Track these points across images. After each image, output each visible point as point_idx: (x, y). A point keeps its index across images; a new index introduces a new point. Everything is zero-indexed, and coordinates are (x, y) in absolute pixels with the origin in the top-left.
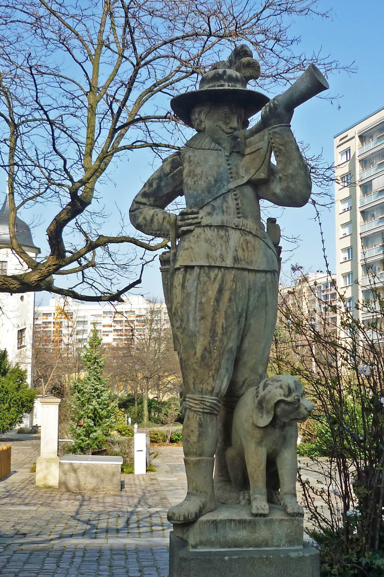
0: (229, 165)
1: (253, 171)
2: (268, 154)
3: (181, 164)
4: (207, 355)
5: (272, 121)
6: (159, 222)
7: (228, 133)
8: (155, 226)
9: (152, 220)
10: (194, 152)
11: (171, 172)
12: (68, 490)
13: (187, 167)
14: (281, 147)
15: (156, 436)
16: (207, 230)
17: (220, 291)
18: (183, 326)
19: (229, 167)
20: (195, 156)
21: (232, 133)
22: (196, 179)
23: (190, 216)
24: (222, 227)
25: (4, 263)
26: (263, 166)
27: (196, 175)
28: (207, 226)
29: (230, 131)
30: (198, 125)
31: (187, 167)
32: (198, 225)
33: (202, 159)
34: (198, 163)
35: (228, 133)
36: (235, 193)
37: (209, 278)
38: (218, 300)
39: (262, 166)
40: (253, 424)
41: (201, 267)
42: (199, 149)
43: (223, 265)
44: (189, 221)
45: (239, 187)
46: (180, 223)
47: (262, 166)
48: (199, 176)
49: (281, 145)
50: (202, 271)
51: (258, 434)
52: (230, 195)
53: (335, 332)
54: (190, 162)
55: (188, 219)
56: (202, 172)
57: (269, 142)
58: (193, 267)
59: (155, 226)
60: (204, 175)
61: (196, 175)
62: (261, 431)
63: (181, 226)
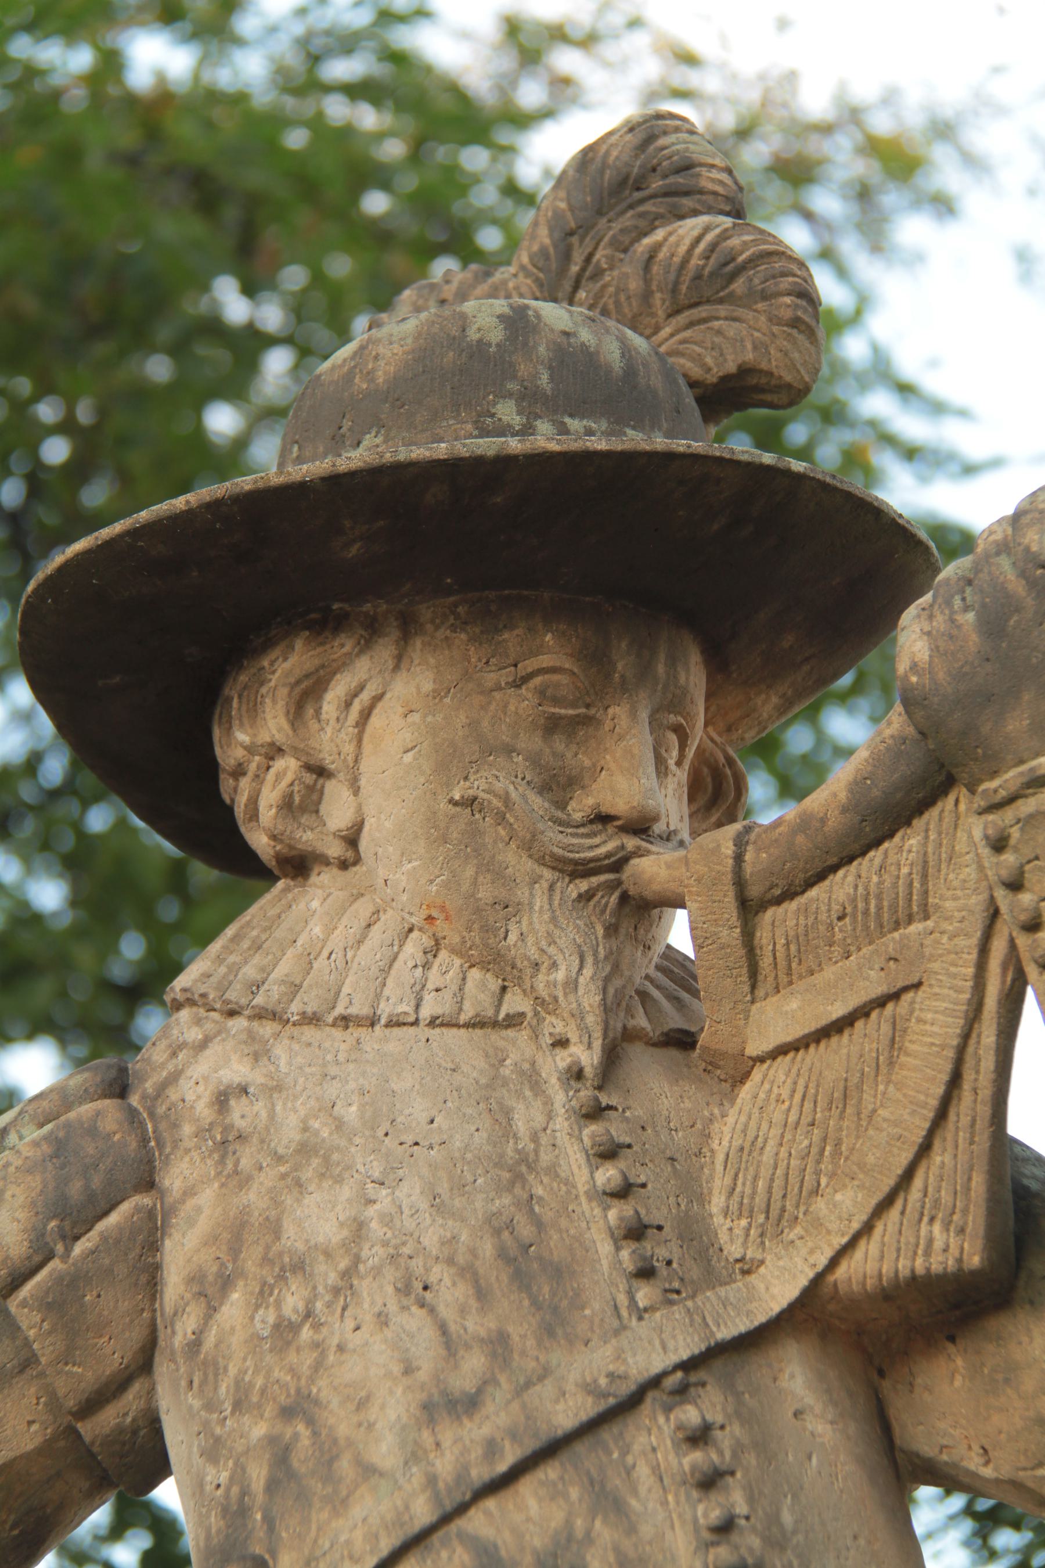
0: (609, 1153)
2: (988, 1035)
4: (438, 1022)
7: (580, 870)
10: (259, 1054)
13: (207, 1197)
15: (561, 829)
19: (608, 1175)
20: (275, 1088)
21: (618, 864)
26: (939, 1157)
27: (299, 1266)
29: (606, 845)
30: (287, 806)
31: (207, 1197)
33: (351, 1113)
34: (305, 1149)
35: (580, 870)
36: (690, 1415)
39: (925, 1149)
42: (312, 1020)
45: (718, 1364)
47: (925, 1149)
48: (328, 1274)
52: (640, 1441)
53: (218, 1248)
56: (359, 1229)
57: (995, 914)
60: (373, 1254)
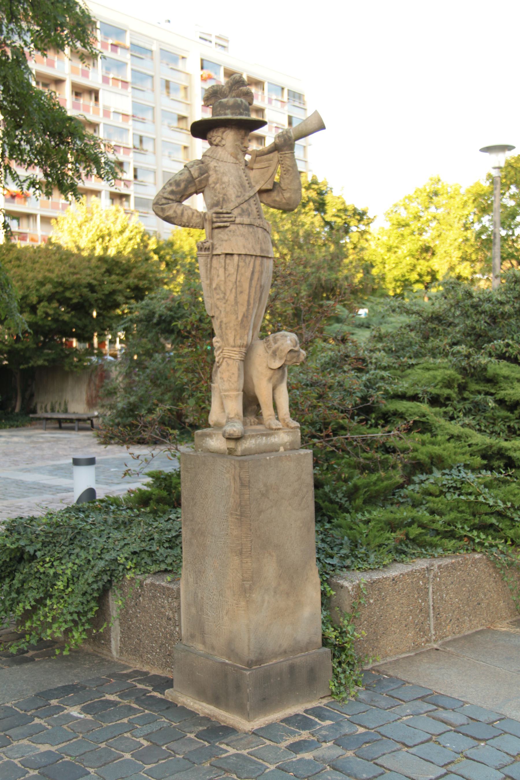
1: (263, 182)
3: (206, 172)
5: (285, 149)
6: (189, 216)
8: (185, 219)
9: (182, 214)
11: (199, 177)
12: (392, 351)
14: (290, 168)
16: (239, 226)
17: (253, 273)
18: (226, 298)
22: (224, 186)
23: (226, 215)
24: (251, 225)
25: (265, 260)
28: (239, 224)
32: (233, 222)
37: (245, 263)
38: (251, 279)
40: (267, 365)
41: (239, 255)
43: (255, 254)
44: (225, 219)
46: (215, 220)
49: (289, 166)
50: (240, 257)
51: (269, 373)
54: (216, 171)
55: (224, 217)
58: (232, 255)
59: (185, 219)
61: (224, 183)
62: (272, 372)
63: (216, 222)
